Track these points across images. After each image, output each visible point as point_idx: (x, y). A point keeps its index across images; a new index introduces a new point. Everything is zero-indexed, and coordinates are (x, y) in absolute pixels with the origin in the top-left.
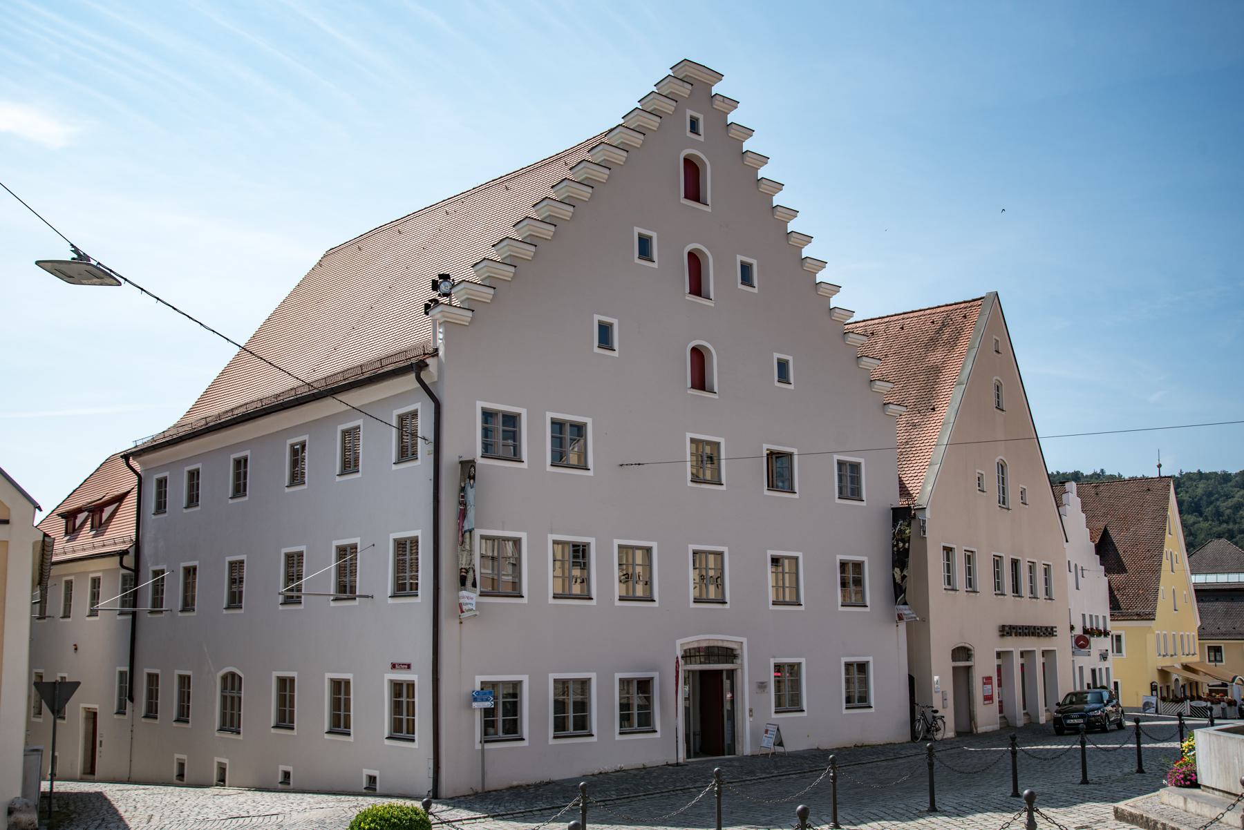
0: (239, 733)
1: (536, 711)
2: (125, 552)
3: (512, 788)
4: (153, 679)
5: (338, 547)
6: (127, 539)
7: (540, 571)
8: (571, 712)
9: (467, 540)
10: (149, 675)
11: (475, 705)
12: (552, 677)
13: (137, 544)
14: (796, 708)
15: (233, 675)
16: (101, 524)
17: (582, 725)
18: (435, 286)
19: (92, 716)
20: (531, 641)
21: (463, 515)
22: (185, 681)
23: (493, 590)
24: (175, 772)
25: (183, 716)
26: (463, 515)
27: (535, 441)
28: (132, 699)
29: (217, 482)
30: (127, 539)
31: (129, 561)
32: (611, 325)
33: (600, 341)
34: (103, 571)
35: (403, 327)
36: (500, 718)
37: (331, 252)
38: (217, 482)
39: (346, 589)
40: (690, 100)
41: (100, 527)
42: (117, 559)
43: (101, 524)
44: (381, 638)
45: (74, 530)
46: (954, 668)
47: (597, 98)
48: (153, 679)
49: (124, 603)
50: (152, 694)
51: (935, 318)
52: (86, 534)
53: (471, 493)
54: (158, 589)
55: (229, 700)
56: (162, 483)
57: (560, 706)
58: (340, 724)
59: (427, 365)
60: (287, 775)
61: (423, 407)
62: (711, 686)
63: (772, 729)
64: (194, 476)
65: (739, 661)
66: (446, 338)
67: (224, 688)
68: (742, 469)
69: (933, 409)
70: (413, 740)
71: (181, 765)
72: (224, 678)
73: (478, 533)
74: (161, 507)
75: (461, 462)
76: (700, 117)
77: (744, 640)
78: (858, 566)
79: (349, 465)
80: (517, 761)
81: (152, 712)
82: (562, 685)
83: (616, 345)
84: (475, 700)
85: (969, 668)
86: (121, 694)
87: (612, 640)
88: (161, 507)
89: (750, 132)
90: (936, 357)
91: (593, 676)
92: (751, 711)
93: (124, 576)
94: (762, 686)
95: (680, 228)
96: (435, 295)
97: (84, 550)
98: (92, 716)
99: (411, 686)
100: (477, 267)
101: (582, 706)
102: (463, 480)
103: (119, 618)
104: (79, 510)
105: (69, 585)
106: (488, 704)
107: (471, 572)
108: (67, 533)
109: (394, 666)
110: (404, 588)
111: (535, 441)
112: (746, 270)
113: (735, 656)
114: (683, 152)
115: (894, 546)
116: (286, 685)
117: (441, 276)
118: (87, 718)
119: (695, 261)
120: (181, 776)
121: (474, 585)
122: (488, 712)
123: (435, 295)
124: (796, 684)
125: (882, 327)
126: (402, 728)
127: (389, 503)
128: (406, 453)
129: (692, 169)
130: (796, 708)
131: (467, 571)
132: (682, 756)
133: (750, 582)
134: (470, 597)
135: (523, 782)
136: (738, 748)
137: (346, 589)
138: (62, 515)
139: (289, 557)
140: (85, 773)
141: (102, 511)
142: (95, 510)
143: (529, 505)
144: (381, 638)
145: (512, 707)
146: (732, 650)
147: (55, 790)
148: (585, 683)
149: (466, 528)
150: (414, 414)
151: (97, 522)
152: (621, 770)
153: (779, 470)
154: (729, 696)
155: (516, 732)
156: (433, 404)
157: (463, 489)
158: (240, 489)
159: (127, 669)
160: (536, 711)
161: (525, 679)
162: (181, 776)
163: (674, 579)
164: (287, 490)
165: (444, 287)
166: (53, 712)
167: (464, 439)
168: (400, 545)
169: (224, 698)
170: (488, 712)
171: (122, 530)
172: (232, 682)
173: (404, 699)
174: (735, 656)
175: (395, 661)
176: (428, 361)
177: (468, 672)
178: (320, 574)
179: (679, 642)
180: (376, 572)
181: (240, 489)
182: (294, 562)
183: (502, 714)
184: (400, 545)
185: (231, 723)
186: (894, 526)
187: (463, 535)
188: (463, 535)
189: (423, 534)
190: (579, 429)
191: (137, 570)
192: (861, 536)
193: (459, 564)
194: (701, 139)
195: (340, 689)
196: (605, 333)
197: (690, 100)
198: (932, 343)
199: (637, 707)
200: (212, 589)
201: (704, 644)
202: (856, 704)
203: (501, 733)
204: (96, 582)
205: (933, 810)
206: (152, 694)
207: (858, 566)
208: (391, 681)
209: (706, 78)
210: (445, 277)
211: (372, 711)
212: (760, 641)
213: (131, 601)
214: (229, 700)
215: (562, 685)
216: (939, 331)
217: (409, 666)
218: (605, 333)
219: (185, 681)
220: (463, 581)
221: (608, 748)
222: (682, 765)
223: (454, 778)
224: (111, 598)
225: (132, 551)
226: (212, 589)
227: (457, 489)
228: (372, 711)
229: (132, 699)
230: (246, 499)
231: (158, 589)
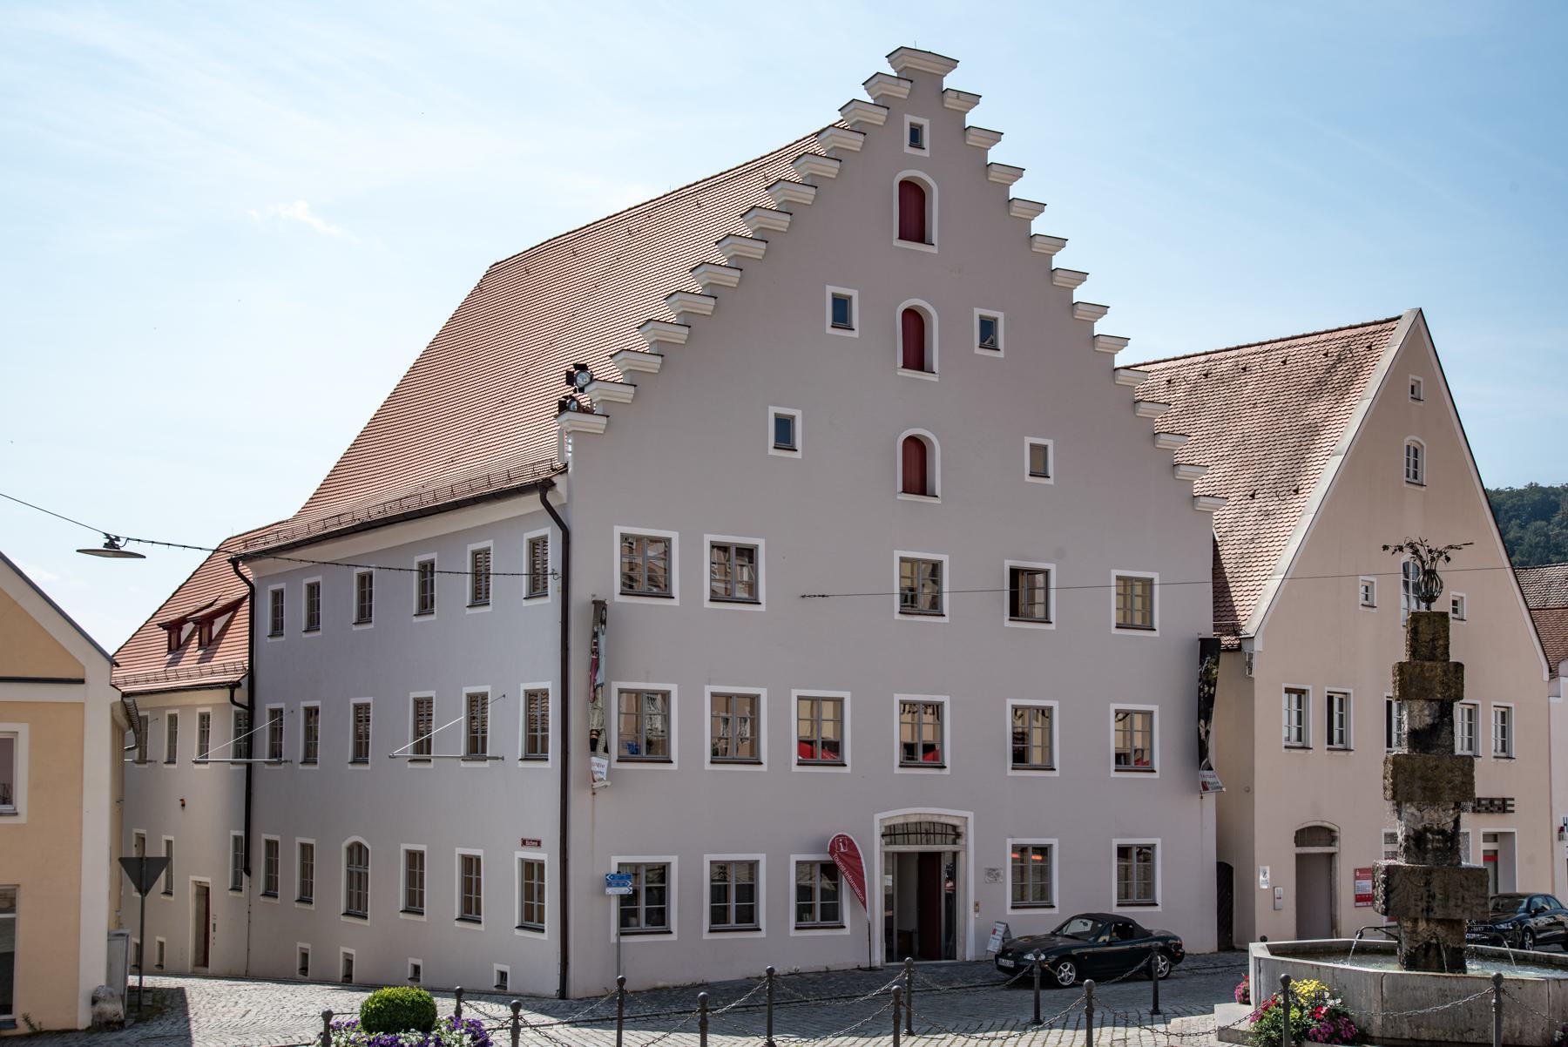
0: (365, 917)
1: (688, 898)
2: (237, 685)
3: (656, 989)
4: (272, 847)
5: (468, 695)
6: (239, 666)
7: (691, 729)
8: (733, 900)
10: (268, 842)
11: (609, 891)
12: (708, 858)
13: (251, 673)
14: (1044, 902)
15: (360, 846)
16: (210, 640)
17: (747, 917)
18: (570, 379)
19: (204, 893)
20: (681, 816)
21: (595, 666)
22: (307, 850)
23: (632, 752)
24: (298, 965)
25: (306, 897)
26: (595, 666)
27: (692, 572)
28: (248, 873)
29: (340, 602)
30: (239, 666)
31: (241, 695)
32: (793, 418)
33: (778, 439)
34: (212, 705)
35: (530, 438)
36: (642, 906)
37: (496, 270)
38: (340, 602)
39: (476, 746)
40: (917, 88)
41: (209, 645)
42: (227, 691)
43: (210, 640)
44: (502, 811)
45: (179, 646)
46: (1299, 856)
47: (798, 94)
48: (272, 847)
49: (238, 754)
50: (272, 866)
51: (1331, 347)
52: (193, 651)
53: (602, 639)
54: (276, 732)
55: (355, 876)
56: (278, 596)
57: (719, 893)
58: (471, 910)
59: (554, 484)
60: (417, 969)
62: (926, 878)
63: (1001, 929)
64: (314, 590)
65: (961, 841)
66: (575, 445)
67: (350, 863)
68: (974, 591)
69: (1296, 491)
70: (542, 931)
71: (305, 956)
72: (350, 849)
73: (616, 686)
74: (277, 628)
75: (594, 602)
76: (925, 123)
77: (970, 815)
79: (480, 596)
80: (656, 959)
81: (271, 891)
82: (721, 869)
83: (798, 444)
84: (609, 885)
85: (1332, 855)
86: (236, 865)
87: (772, 819)
88: (277, 628)
89: (996, 136)
90: (1316, 411)
91: (762, 858)
92: (977, 904)
93: (237, 714)
94: (993, 873)
95: (892, 277)
96: (569, 390)
97: (189, 676)
98: (204, 893)
99: (541, 866)
100: (697, 272)
101: (748, 892)
102: (595, 624)
103: (232, 767)
104: (183, 621)
105: (173, 720)
106: (626, 890)
107: (602, 737)
108: (170, 650)
109: (524, 842)
110: (535, 748)
111: (692, 572)
112: (988, 327)
113: (958, 835)
114: (908, 172)
115: (1201, 690)
116: (415, 859)
117: (577, 366)
118: (198, 894)
119: (914, 322)
120: (304, 970)
121: (606, 750)
122: (624, 900)
123: (569, 390)
124: (1044, 872)
125: (1259, 359)
126: (531, 918)
127: (511, 647)
128: (537, 588)
129: (913, 196)
130: (1044, 902)
131: (599, 733)
132: (878, 958)
134: (600, 764)
135: (670, 984)
137: (476, 746)
138: (164, 626)
139: (419, 703)
140: (197, 965)
141: (212, 624)
142: (205, 622)
143: (682, 653)
144: (502, 811)
145: (658, 895)
148: (752, 866)
149: (599, 682)
150: (544, 540)
151: (205, 639)
152: (797, 973)
153: (1023, 593)
155: (836, 918)
156: (560, 533)
157: (596, 635)
158: (364, 615)
159: (242, 833)
160: (688, 898)
161: (673, 860)
162: (304, 970)
164: (415, 620)
165: (582, 379)
166: (140, 891)
167: (599, 572)
168: (531, 696)
169: (350, 874)
170: (624, 900)
171: (232, 655)
172: (358, 854)
173: (535, 882)
174: (958, 835)
175: (527, 837)
176: (555, 480)
177: (606, 848)
178: (450, 727)
179: (878, 817)
180: (506, 729)
181: (364, 615)
182: (423, 709)
183: (644, 901)
184: (531, 696)
185: (357, 907)
186: (1201, 663)
187: (595, 690)
188: (595, 690)
189: (551, 685)
190: (748, 553)
191: (251, 707)
192: (1149, 677)
193: (601, 725)
194: (926, 153)
195: (471, 865)
196: (784, 427)
197: (917, 88)
198: (1318, 388)
199: (820, 896)
200: (337, 736)
201: (914, 820)
202: (1135, 899)
203: (643, 924)
204: (205, 718)
205: (1037, 1021)
206: (272, 866)
208: (523, 860)
209: (931, 68)
210: (582, 368)
211: (502, 894)
212: (987, 813)
213: (245, 749)
214: (1336, 701)
215: (721, 869)
216: (1331, 370)
217: (539, 843)
218: (784, 427)
219: (307, 850)
220: (593, 745)
221: (780, 942)
223: (588, 976)
224: (223, 741)
225: (245, 683)
226: (337, 736)
227: (590, 634)
228: (502, 894)
229: (248, 873)
230: (371, 626)
231: (276, 732)
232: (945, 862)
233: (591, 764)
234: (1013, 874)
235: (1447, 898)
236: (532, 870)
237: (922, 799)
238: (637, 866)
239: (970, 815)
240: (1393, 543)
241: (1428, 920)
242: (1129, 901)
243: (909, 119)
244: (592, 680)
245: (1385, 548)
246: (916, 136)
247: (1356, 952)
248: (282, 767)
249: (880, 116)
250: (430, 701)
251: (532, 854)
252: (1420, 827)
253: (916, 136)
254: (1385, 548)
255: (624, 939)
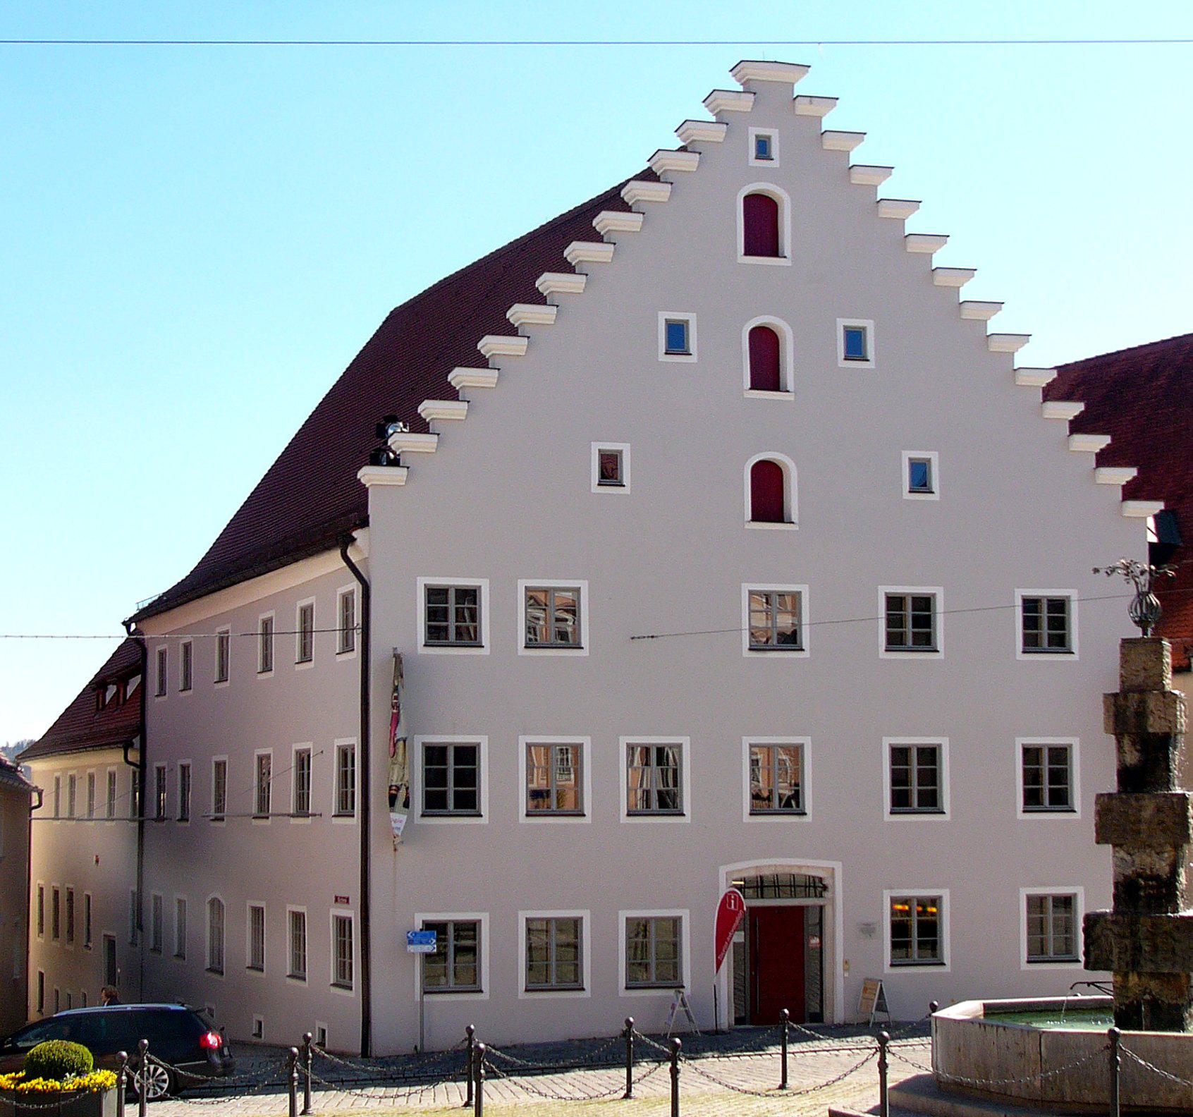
9: (400, 751)
11: (411, 948)
12: (623, 915)
21: (395, 720)
26: (395, 720)
59: (354, 539)
61: (355, 586)
70: (351, 989)
78: (1060, 755)
84: (411, 942)
92: (846, 962)
106: (431, 948)
111: (501, 619)
113: (825, 888)
116: (298, 919)
121: (406, 804)
130: (932, 960)
131: (398, 789)
133: (850, 783)
134: (398, 818)
136: (827, 1014)
139: (260, 759)
146: (821, 879)
147: (337, 553)
154: (815, 941)
157: (396, 689)
161: (586, 915)
163: (716, 786)
177: (406, 903)
187: (396, 744)
188: (396, 744)
189: (356, 741)
194: (774, 164)
207: (1060, 755)
220: (392, 800)
222: (723, 1032)
232: (812, 919)
233: (390, 821)
234: (1029, 927)
235: (1155, 948)
236: (343, 925)
237: (780, 849)
238: (548, 921)
239: (838, 866)
240: (1103, 565)
241: (1140, 975)
242: (1045, 957)
243: (754, 132)
244: (393, 733)
245: (1096, 571)
246: (763, 148)
247: (1068, 1010)
248: (269, 822)
249: (719, 133)
250: (268, 757)
251: (344, 912)
252: (1129, 872)
253: (763, 148)
254: (1096, 571)
255: (426, 998)
